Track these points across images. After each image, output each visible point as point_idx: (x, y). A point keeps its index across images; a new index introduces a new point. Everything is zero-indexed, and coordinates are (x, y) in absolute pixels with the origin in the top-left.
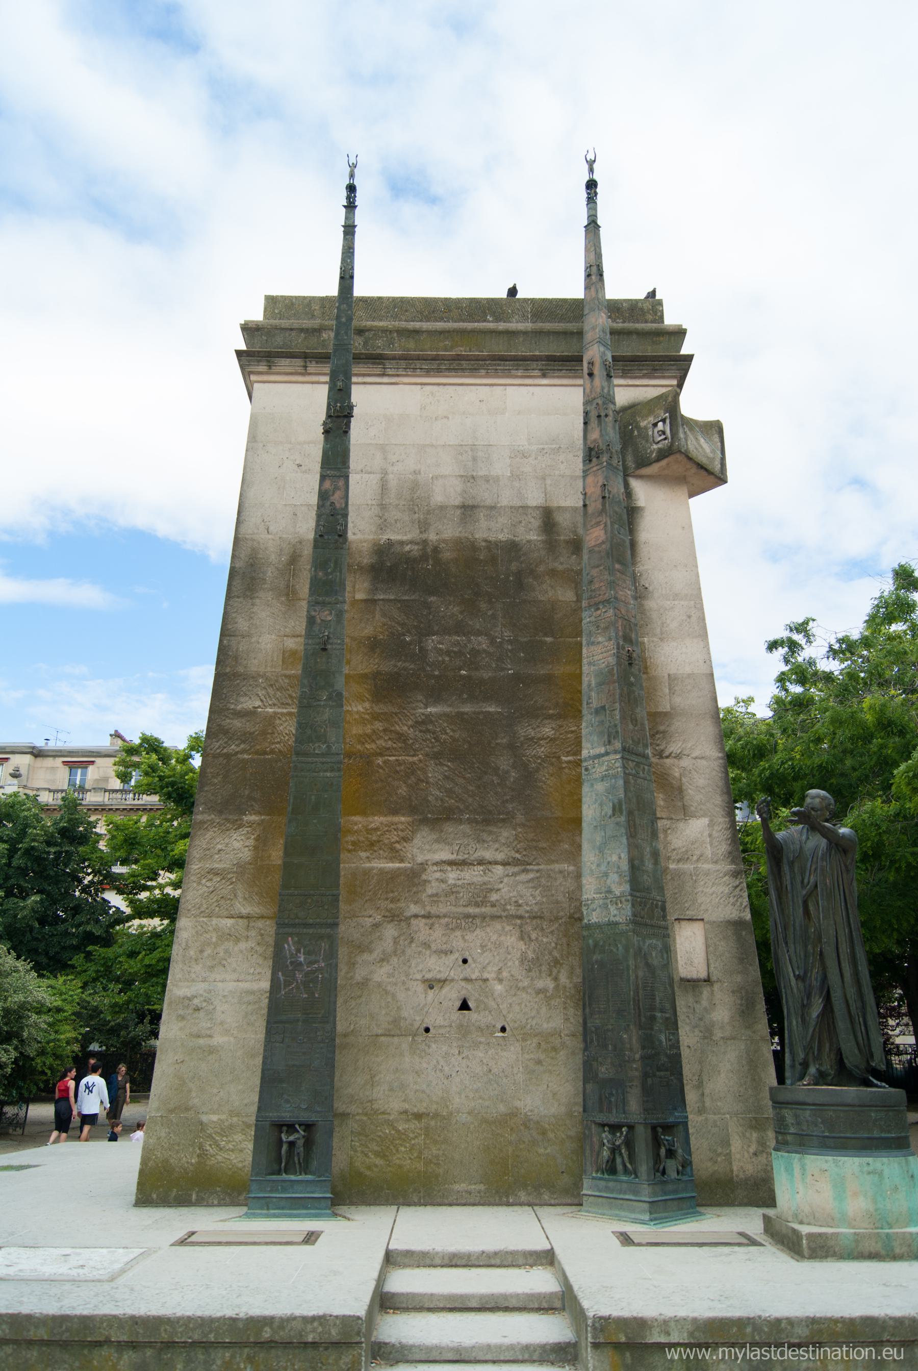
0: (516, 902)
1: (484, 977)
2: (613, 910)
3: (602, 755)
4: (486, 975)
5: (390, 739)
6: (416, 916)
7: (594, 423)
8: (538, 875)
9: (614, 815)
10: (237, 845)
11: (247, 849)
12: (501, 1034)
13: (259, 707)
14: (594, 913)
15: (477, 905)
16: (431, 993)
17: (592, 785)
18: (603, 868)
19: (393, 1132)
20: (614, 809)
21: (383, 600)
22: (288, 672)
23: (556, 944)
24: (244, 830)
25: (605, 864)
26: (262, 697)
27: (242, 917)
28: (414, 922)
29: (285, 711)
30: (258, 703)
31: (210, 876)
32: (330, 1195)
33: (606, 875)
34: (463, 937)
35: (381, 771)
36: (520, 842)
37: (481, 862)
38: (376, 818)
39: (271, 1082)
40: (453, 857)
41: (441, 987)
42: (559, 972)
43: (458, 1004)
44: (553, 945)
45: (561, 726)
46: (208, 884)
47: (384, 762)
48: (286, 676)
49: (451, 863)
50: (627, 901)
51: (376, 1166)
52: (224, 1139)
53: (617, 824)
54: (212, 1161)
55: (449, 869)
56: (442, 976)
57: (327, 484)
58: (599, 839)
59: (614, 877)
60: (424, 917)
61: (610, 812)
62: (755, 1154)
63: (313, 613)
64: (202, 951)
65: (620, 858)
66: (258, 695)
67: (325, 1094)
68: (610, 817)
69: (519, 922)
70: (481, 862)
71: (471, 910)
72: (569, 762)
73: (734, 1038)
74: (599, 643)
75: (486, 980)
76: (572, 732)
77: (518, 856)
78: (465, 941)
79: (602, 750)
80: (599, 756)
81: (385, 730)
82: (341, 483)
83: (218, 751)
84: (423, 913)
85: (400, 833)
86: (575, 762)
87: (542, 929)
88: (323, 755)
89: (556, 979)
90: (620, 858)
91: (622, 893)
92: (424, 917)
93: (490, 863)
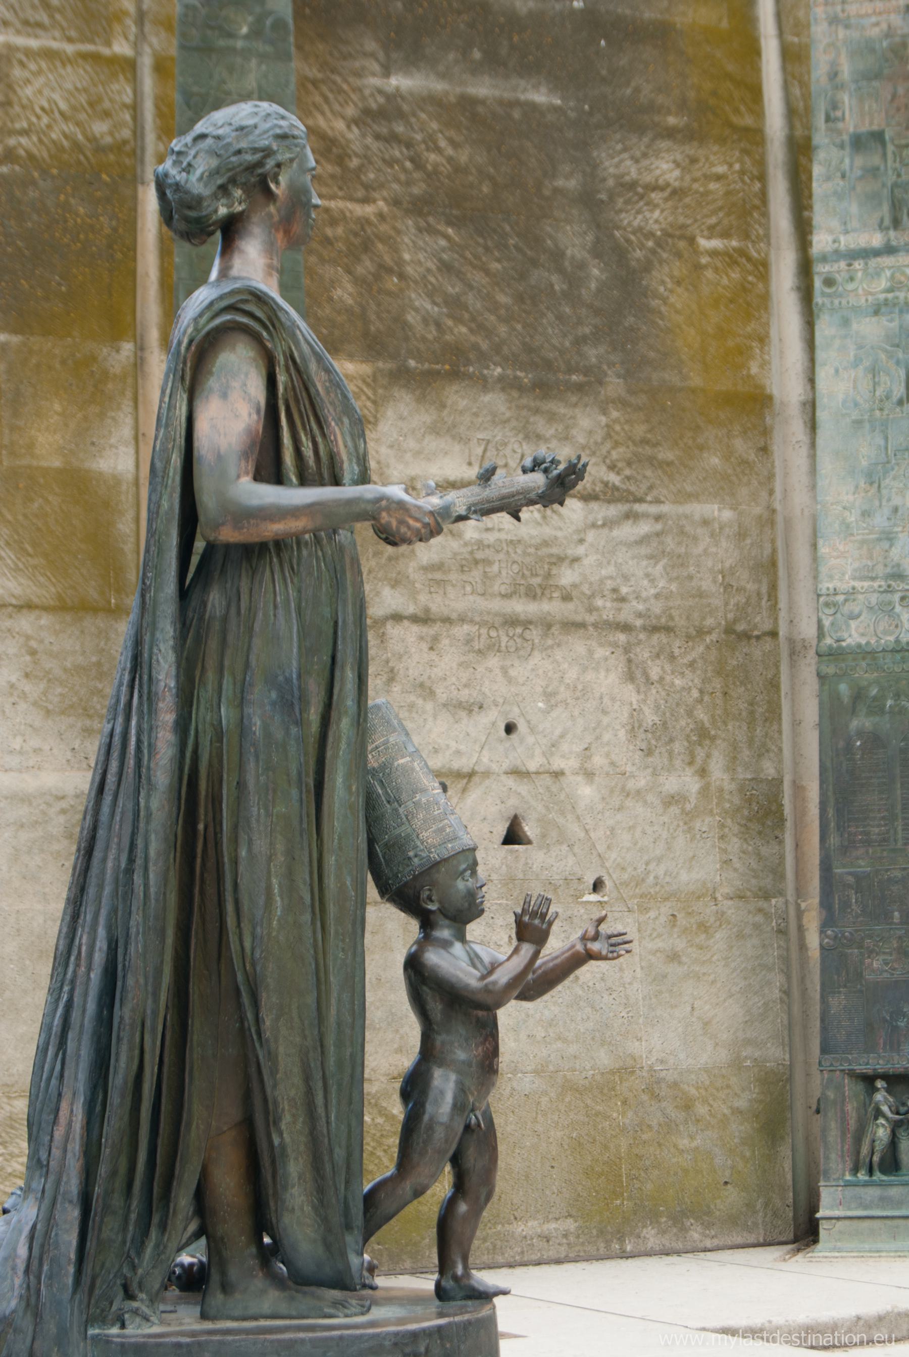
3: (877, 253)
4: (558, 763)
6: (397, 618)
8: (659, 527)
12: (594, 897)
14: (853, 624)
15: (532, 594)
17: (846, 322)
18: (880, 520)
19: (380, 1120)
23: (701, 692)
25: (886, 511)
29: (34, 43)
34: (504, 671)
36: (617, 444)
41: (464, 790)
42: (708, 756)
43: (501, 830)
44: (695, 694)
45: (693, 160)
58: (866, 450)
69: (622, 637)
71: (521, 607)
72: (714, 253)
75: (558, 775)
76: (718, 178)
77: (614, 479)
78: (510, 681)
79: (877, 240)
84: (411, 609)
86: (726, 253)
87: (672, 658)
89: (703, 772)
92: (415, 619)
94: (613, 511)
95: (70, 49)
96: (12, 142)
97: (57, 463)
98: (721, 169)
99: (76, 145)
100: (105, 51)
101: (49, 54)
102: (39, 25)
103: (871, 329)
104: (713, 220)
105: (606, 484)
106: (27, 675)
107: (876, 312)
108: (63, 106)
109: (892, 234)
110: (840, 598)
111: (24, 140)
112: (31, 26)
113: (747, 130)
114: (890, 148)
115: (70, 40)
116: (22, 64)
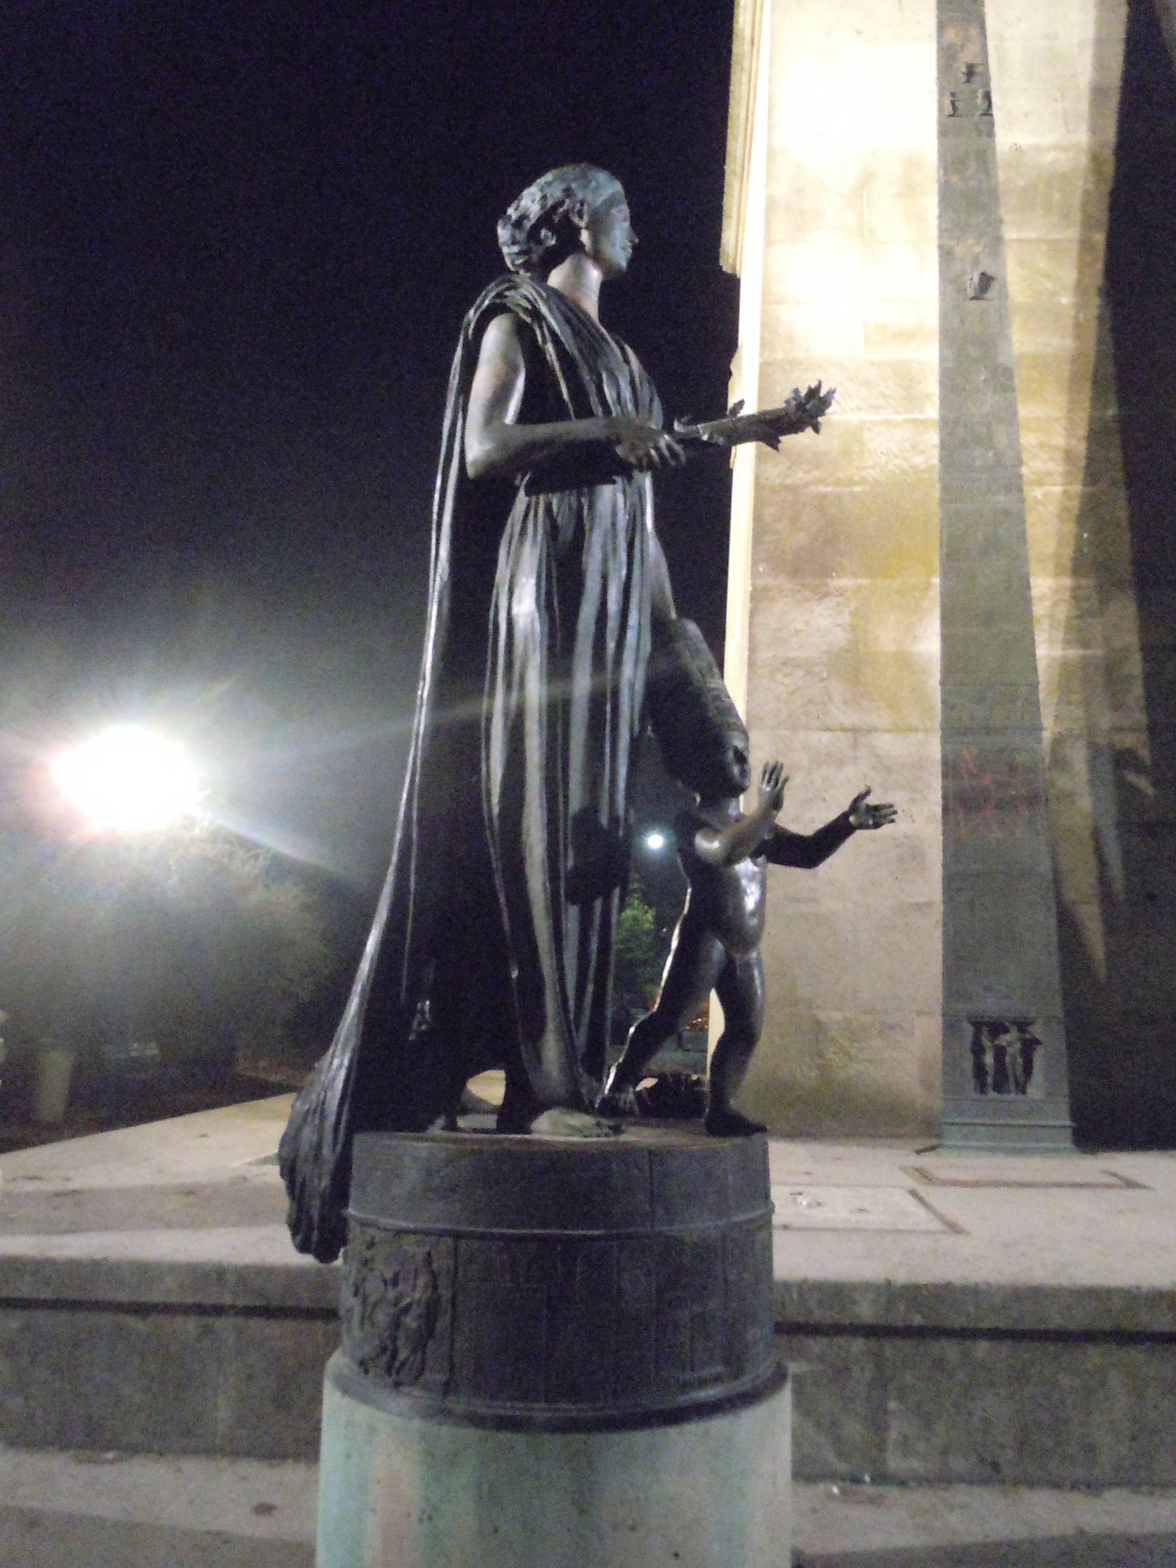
5: (1051, 459)
11: (839, 629)
21: (1020, 241)
24: (832, 601)
46: (786, 681)
47: (1045, 495)
48: (872, 364)
52: (857, 1045)
54: (842, 1075)
82: (974, 31)
96: (864, 473)
97: (893, 648)
99: (904, 472)
100: (921, 417)
101: (887, 423)
108: (895, 450)
111: (871, 472)
115: (899, 413)
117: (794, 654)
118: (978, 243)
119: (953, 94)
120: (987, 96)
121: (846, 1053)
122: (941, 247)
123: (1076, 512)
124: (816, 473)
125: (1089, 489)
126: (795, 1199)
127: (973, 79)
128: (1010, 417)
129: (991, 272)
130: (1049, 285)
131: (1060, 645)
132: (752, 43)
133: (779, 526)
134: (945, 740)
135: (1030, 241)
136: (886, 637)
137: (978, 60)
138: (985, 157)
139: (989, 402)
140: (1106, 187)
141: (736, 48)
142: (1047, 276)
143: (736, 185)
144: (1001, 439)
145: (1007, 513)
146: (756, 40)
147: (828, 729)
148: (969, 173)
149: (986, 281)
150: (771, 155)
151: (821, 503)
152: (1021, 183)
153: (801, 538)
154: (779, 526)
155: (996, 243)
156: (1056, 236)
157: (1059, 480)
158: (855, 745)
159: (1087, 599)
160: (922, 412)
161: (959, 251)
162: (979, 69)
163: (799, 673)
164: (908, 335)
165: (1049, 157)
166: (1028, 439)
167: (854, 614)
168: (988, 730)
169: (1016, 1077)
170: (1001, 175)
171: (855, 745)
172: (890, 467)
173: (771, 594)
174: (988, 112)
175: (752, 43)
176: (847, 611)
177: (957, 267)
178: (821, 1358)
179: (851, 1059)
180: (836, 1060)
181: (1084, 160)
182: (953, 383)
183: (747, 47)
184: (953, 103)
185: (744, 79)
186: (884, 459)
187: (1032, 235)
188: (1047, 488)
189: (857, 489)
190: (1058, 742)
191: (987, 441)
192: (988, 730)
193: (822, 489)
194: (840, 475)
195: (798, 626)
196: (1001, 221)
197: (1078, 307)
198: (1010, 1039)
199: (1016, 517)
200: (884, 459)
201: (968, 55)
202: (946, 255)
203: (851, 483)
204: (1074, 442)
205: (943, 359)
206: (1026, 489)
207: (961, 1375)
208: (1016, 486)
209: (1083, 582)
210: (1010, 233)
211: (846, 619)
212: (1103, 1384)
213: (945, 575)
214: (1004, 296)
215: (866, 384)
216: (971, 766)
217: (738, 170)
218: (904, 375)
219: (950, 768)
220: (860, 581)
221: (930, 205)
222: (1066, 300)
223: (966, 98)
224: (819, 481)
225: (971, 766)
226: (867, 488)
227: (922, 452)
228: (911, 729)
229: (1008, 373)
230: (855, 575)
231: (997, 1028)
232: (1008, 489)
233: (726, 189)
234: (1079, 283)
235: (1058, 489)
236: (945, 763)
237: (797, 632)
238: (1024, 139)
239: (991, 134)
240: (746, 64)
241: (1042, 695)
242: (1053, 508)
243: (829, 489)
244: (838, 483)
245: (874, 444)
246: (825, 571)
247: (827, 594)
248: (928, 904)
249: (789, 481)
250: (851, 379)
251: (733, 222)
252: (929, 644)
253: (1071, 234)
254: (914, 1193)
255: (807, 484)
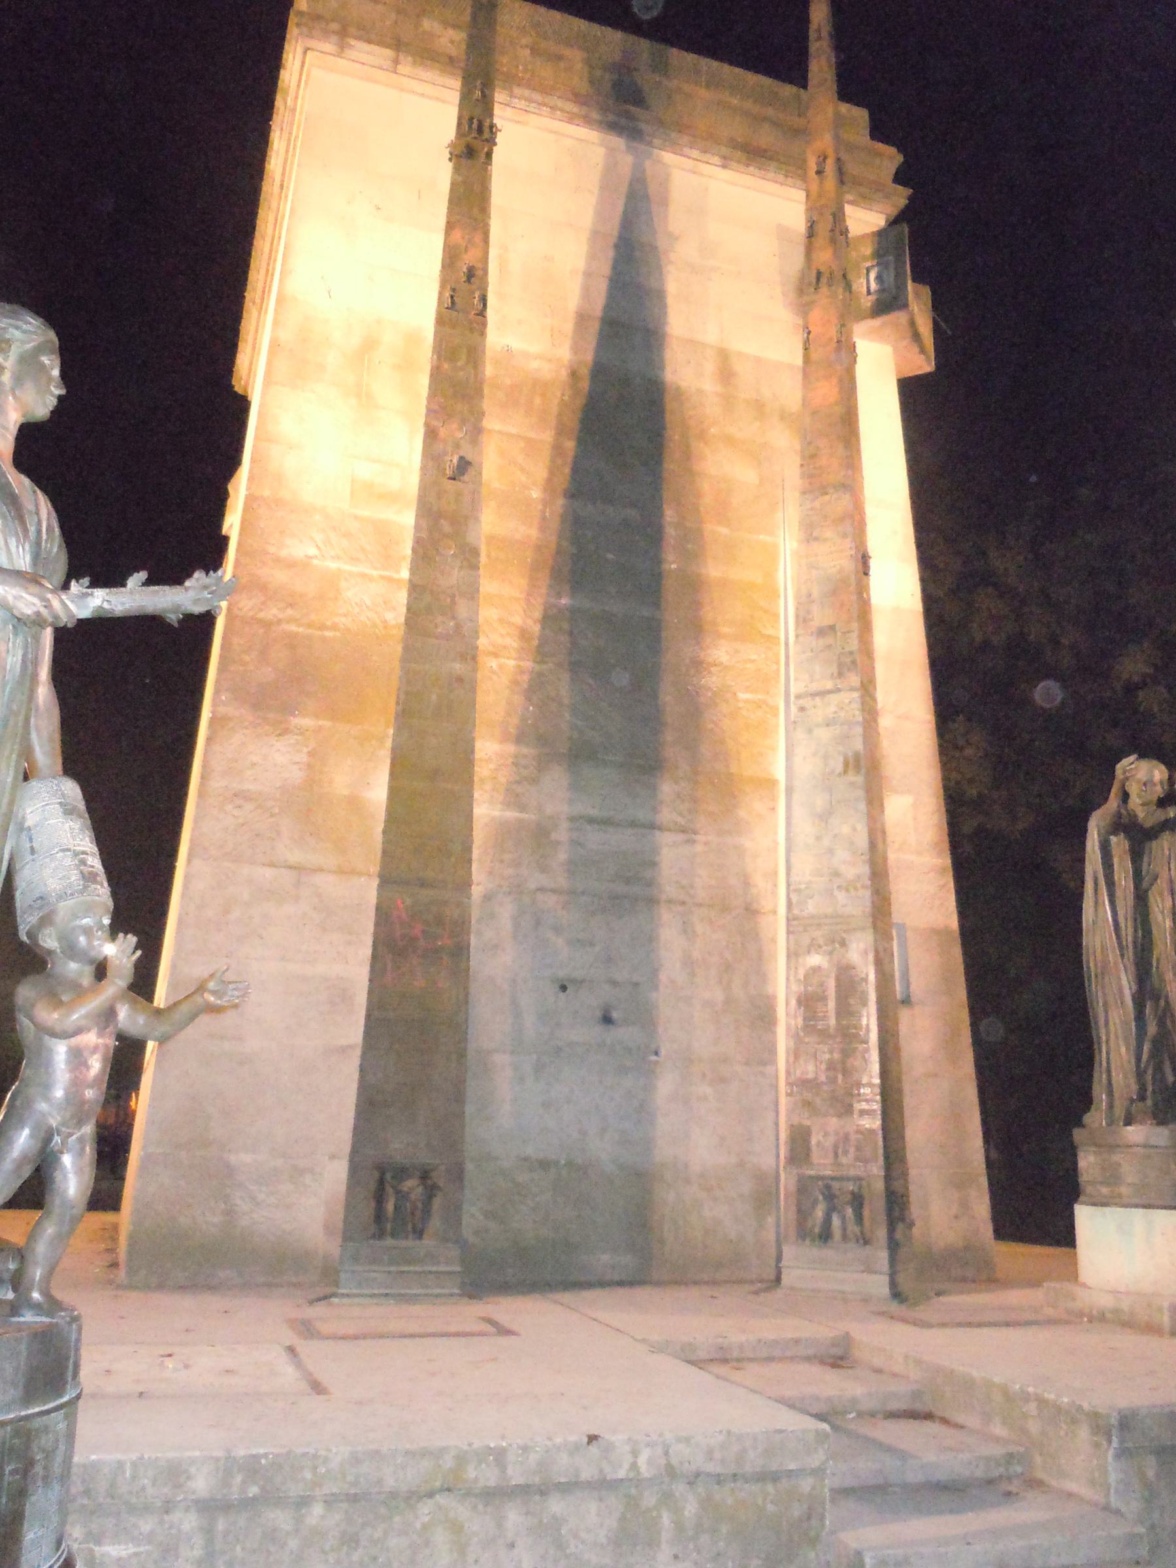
0: (677, 882)
1: (635, 979)
2: (841, 897)
3: (830, 692)
4: (635, 978)
5: (508, 634)
7: (821, 240)
9: (845, 772)
10: (280, 759)
11: (296, 767)
13: (316, 557)
14: (810, 901)
16: (562, 995)
17: (810, 731)
18: (826, 842)
20: (846, 764)
21: (500, 432)
22: (359, 512)
24: (292, 739)
26: (320, 544)
27: (290, 867)
28: (540, 897)
29: (354, 569)
30: (312, 551)
31: (238, 802)
32: (458, 1269)
33: (831, 851)
35: (495, 677)
37: (633, 824)
38: (488, 744)
39: (372, 1105)
40: (594, 813)
43: (599, 1014)
45: (737, 651)
46: (236, 812)
47: (501, 667)
48: (356, 517)
49: (591, 821)
50: (863, 887)
51: (487, 1231)
52: (264, 1189)
53: (852, 784)
54: (244, 1222)
55: (589, 827)
56: (578, 974)
57: (457, 235)
58: (820, 801)
59: (842, 854)
60: (553, 891)
61: (840, 768)
62: (956, 1217)
63: (435, 423)
64: (227, 912)
65: (854, 829)
66: (312, 539)
67: (450, 1128)
68: (840, 775)
69: (680, 908)
70: (633, 824)
71: (620, 888)
72: (747, 701)
73: (936, 1075)
74: (826, 540)
75: (636, 984)
76: (753, 661)
77: (679, 820)
79: (829, 685)
80: (822, 694)
81: (501, 621)
82: (478, 238)
83: (251, 614)
85: (522, 770)
87: (711, 922)
88: (447, 637)
90: (854, 829)
91: (859, 877)
92: (553, 891)
93: (643, 826)
94: (680, 837)
95: (375, 573)
96: (336, 620)
97: (346, 792)
98: (754, 657)
99: (375, 625)
100: (396, 576)
101: (363, 576)
102: (357, 560)
103: (824, 734)
104: (748, 684)
105: (676, 823)
106: (315, 908)
107: (828, 725)
108: (368, 602)
109: (838, 681)
110: (803, 886)
111: (343, 619)
112: (354, 560)
113: (769, 636)
114: (839, 634)
115: (376, 569)
116: (346, 579)
117: (248, 786)
118: (461, 429)
119: (454, 290)
120: (484, 300)
121: (253, 1199)
122: (427, 424)
123: (525, 686)
124: (289, 612)
125: (537, 668)
126: (162, 1364)
127: (473, 280)
128: (472, 593)
129: (469, 457)
130: (523, 479)
131: (499, 806)
132: (282, 186)
133: (247, 658)
134: (381, 886)
135: (510, 435)
136: (340, 779)
137: (480, 265)
138: (475, 354)
139: (454, 576)
140: (580, 401)
141: (266, 187)
142: (522, 470)
143: (255, 313)
144: (462, 611)
145: (460, 680)
146: (285, 184)
147: (272, 865)
148: (459, 364)
149: (464, 466)
150: (280, 300)
151: (292, 642)
152: (508, 382)
153: (266, 674)
154: (247, 658)
155: (477, 433)
156: (532, 435)
157: (514, 654)
158: (298, 884)
159: (525, 767)
160: (398, 572)
161: (443, 432)
162: (479, 273)
163: (249, 806)
164: (392, 498)
165: (535, 364)
166: (488, 614)
167: (311, 754)
168: (423, 884)
169: (1162, 913)
170: (489, 370)
171: (298, 884)
172: (363, 618)
173: (231, 725)
174: (482, 313)
175: (282, 186)
176: (305, 750)
177: (439, 447)
178: (150, 1538)
179: (258, 1204)
180: (243, 1206)
181: (564, 374)
182: (425, 551)
183: (276, 189)
184: (452, 297)
185: (271, 218)
186: (357, 610)
187: (514, 431)
188: (502, 660)
189: (328, 634)
190: (488, 897)
191: (449, 610)
192: (423, 884)
193: (293, 628)
194: (313, 617)
195: (255, 759)
196: (483, 414)
197: (545, 503)
198: (411, 1184)
199: (466, 685)
200: (357, 610)
201: (470, 258)
202: (431, 434)
203: (323, 627)
204: (530, 622)
205: (417, 527)
206: (482, 659)
207: (293, 1544)
208: (470, 656)
209: (525, 750)
210: (491, 423)
211: (304, 758)
212: (427, 1543)
213: (399, 729)
214: (478, 481)
215: (348, 535)
216: (404, 915)
217: (258, 301)
218: (383, 531)
219: (383, 915)
220: (320, 723)
221: (423, 381)
222: (536, 494)
223: (464, 297)
224: (290, 620)
225: (404, 915)
226: (338, 634)
227: (394, 609)
228: (353, 872)
229: (475, 552)
230: (317, 716)
231: (402, 1172)
232: (463, 657)
233: (245, 314)
234: (549, 480)
235: (512, 663)
236: (378, 908)
237: (254, 764)
238: (516, 343)
239: (483, 334)
240: (274, 205)
241: (476, 853)
242: (505, 680)
243: (301, 630)
244: (309, 625)
245: (349, 594)
246: (289, 709)
247: (285, 732)
248: (350, 1047)
249: (261, 615)
250: (334, 528)
251: (248, 349)
252: (378, 793)
253: (547, 436)
254: (291, 1350)
255: (279, 621)
